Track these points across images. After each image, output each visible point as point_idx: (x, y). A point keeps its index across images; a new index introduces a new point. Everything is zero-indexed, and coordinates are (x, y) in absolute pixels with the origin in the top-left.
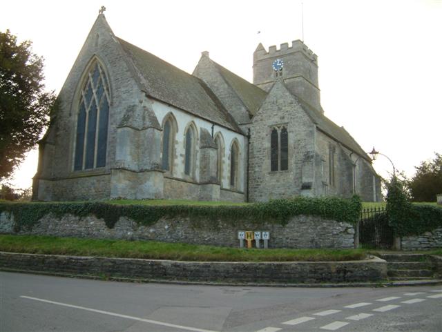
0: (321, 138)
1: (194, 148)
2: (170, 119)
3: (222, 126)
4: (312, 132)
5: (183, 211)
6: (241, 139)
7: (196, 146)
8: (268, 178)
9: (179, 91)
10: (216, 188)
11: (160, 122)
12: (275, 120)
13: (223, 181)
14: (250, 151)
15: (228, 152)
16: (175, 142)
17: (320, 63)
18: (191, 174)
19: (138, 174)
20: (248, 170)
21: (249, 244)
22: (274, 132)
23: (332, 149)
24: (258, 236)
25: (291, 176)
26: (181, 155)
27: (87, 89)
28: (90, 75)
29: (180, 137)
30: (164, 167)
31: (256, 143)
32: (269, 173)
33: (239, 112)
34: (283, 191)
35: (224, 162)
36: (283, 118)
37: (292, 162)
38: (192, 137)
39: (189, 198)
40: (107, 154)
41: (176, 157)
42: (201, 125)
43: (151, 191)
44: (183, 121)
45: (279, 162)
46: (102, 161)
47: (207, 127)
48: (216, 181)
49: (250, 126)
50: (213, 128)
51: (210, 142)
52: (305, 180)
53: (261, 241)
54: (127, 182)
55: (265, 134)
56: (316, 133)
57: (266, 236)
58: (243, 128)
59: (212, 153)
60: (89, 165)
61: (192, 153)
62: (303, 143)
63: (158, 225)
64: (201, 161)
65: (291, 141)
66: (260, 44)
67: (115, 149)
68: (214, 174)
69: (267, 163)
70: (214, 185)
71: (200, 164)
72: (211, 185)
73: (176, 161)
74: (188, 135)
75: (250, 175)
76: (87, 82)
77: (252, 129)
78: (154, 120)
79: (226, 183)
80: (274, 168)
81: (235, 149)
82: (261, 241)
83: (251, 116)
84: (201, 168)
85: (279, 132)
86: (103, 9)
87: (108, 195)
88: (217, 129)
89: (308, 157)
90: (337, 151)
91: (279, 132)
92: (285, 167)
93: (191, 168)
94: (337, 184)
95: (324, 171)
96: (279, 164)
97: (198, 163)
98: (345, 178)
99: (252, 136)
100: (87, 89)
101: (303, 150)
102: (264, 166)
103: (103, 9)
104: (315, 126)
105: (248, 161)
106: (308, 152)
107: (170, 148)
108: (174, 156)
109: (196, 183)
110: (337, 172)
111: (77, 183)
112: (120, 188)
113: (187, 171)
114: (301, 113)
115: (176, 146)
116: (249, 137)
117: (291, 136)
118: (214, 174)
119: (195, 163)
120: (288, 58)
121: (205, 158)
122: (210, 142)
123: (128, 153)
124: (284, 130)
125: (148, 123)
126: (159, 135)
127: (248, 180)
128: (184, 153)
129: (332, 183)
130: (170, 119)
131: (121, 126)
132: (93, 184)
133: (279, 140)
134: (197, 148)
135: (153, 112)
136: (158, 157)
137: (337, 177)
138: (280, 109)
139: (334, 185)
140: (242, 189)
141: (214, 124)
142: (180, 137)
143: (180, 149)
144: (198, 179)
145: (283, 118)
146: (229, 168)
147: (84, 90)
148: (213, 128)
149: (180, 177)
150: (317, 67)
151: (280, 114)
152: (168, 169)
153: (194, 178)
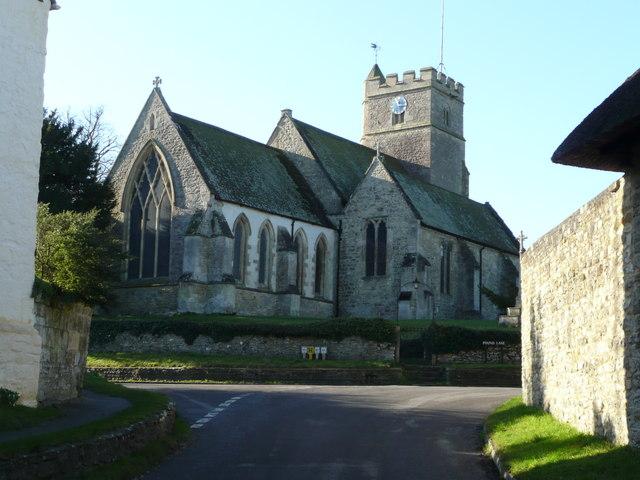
0: (429, 234)
1: (270, 250)
2: (242, 221)
3: (302, 221)
4: (414, 230)
5: (305, 197)
6: (329, 234)
7: (273, 248)
8: (361, 284)
9: (252, 181)
10: (295, 299)
11: (231, 227)
12: (370, 212)
13: (305, 288)
14: (341, 249)
15: (312, 252)
16: (247, 247)
17: (467, 97)
18: (266, 283)
19: (209, 287)
20: (338, 274)
21: (311, 358)
22: (371, 227)
23: (448, 248)
24: (317, 350)
25: (389, 283)
26: (254, 261)
27: (142, 181)
28: (145, 164)
29: (253, 241)
30: (234, 278)
31: (349, 241)
32: (363, 279)
33: (329, 197)
34: (379, 301)
35: (307, 265)
36: (381, 209)
37: (390, 265)
38: (268, 238)
39: (263, 308)
40: (171, 261)
41: (249, 264)
42: (279, 223)
43: (222, 305)
44: (256, 219)
45: (376, 261)
46: (163, 268)
47: (286, 224)
48: (296, 289)
49: (342, 217)
50: (293, 225)
51: (289, 242)
52: (404, 289)
53: (320, 355)
54: (196, 296)
55: (359, 228)
56: (420, 231)
57: (324, 350)
58: (333, 219)
59: (291, 257)
60: (148, 272)
61: (267, 257)
62: (403, 243)
63: (234, 341)
64: (278, 267)
65: (390, 240)
66: (376, 67)
67: (182, 256)
68: (293, 282)
69: (361, 265)
70: (293, 295)
71: (277, 271)
72: (288, 295)
73: (249, 269)
74: (263, 236)
75: (341, 280)
76: (141, 173)
77: (344, 221)
78: (224, 226)
79: (309, 291)
80: (369, 272)
81: (322, 246)
82: (320, 355)
83: (344, 203)
84: (277, 275)
85: (376, 227)
86: (158, 81)
87: (175, 307)
88: (298, 225)
89: (408, 261)
90: (455, 249)
91: (376, 227)
92: (382, 271)
93: (267, 274)
94: (454, 291)
95: (432, 278)
96: (376, 268)
97: (274, 269)
98: (464, 284)
99: (344, 231)
100: (142, 181)
101: (404, 251)
102: (357, 270)
103: (158, 81)
104: (419, 222)
105: (338, 262)
106: (409, 255)
107: (243, 245)
108: (246, 263)
109: (272, 293)
110: (454, 275)
111: (133, 294)
112: (191, 301)
113: (261, 279)
114: (403, 206)
115: (249, 251)
116: (339, 232)
117: (390, 232)
118: (293, 282)
119: (270, 270)
120: (411, 96)
121: (282, 263)
122: (289, 242)
123: (197, 264)
124: (383, 226)
125: (218, 230)
126: (229, 242)
127: (338, 286)
128: (258, 258)
129: (445, 291)
130: (242, 221)
131: (189, 233)
132: (155, 295)
133: (376, 234)
134: (274, 251)
135: (223, 217)
136: (228, 268)
137: (454, 284)
138: (377, 198)
139: (448, 293)
140: (331, 298)
141: (294, 219)
142: (253, 241)
143: (253, 255)
144: (274, 288)
145: (381, 209)
146: (313, 272)
147: (138, 182)
148: (293, 225)
149: (254, 286)
150: (461, 103)
151: (379, 204)
152: (239, 278)
153: (269, 287)
